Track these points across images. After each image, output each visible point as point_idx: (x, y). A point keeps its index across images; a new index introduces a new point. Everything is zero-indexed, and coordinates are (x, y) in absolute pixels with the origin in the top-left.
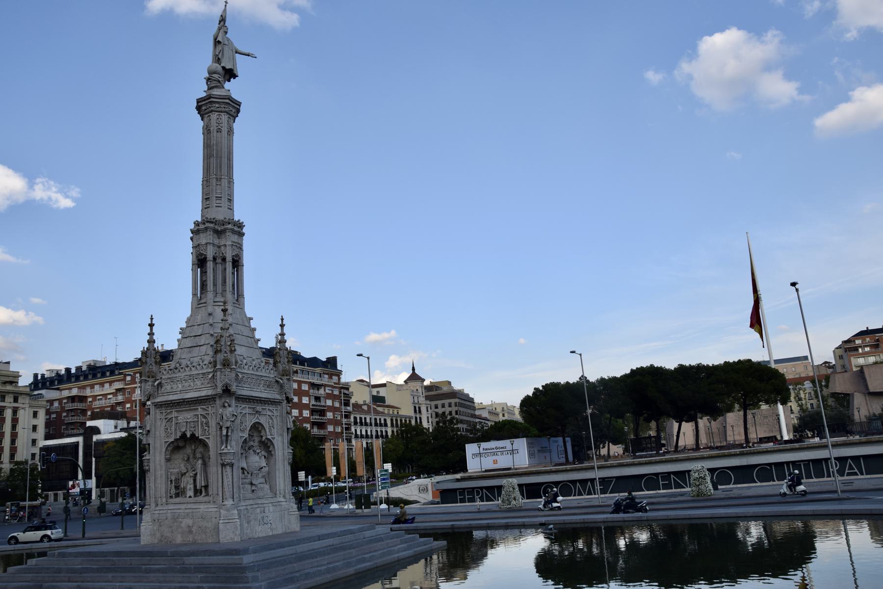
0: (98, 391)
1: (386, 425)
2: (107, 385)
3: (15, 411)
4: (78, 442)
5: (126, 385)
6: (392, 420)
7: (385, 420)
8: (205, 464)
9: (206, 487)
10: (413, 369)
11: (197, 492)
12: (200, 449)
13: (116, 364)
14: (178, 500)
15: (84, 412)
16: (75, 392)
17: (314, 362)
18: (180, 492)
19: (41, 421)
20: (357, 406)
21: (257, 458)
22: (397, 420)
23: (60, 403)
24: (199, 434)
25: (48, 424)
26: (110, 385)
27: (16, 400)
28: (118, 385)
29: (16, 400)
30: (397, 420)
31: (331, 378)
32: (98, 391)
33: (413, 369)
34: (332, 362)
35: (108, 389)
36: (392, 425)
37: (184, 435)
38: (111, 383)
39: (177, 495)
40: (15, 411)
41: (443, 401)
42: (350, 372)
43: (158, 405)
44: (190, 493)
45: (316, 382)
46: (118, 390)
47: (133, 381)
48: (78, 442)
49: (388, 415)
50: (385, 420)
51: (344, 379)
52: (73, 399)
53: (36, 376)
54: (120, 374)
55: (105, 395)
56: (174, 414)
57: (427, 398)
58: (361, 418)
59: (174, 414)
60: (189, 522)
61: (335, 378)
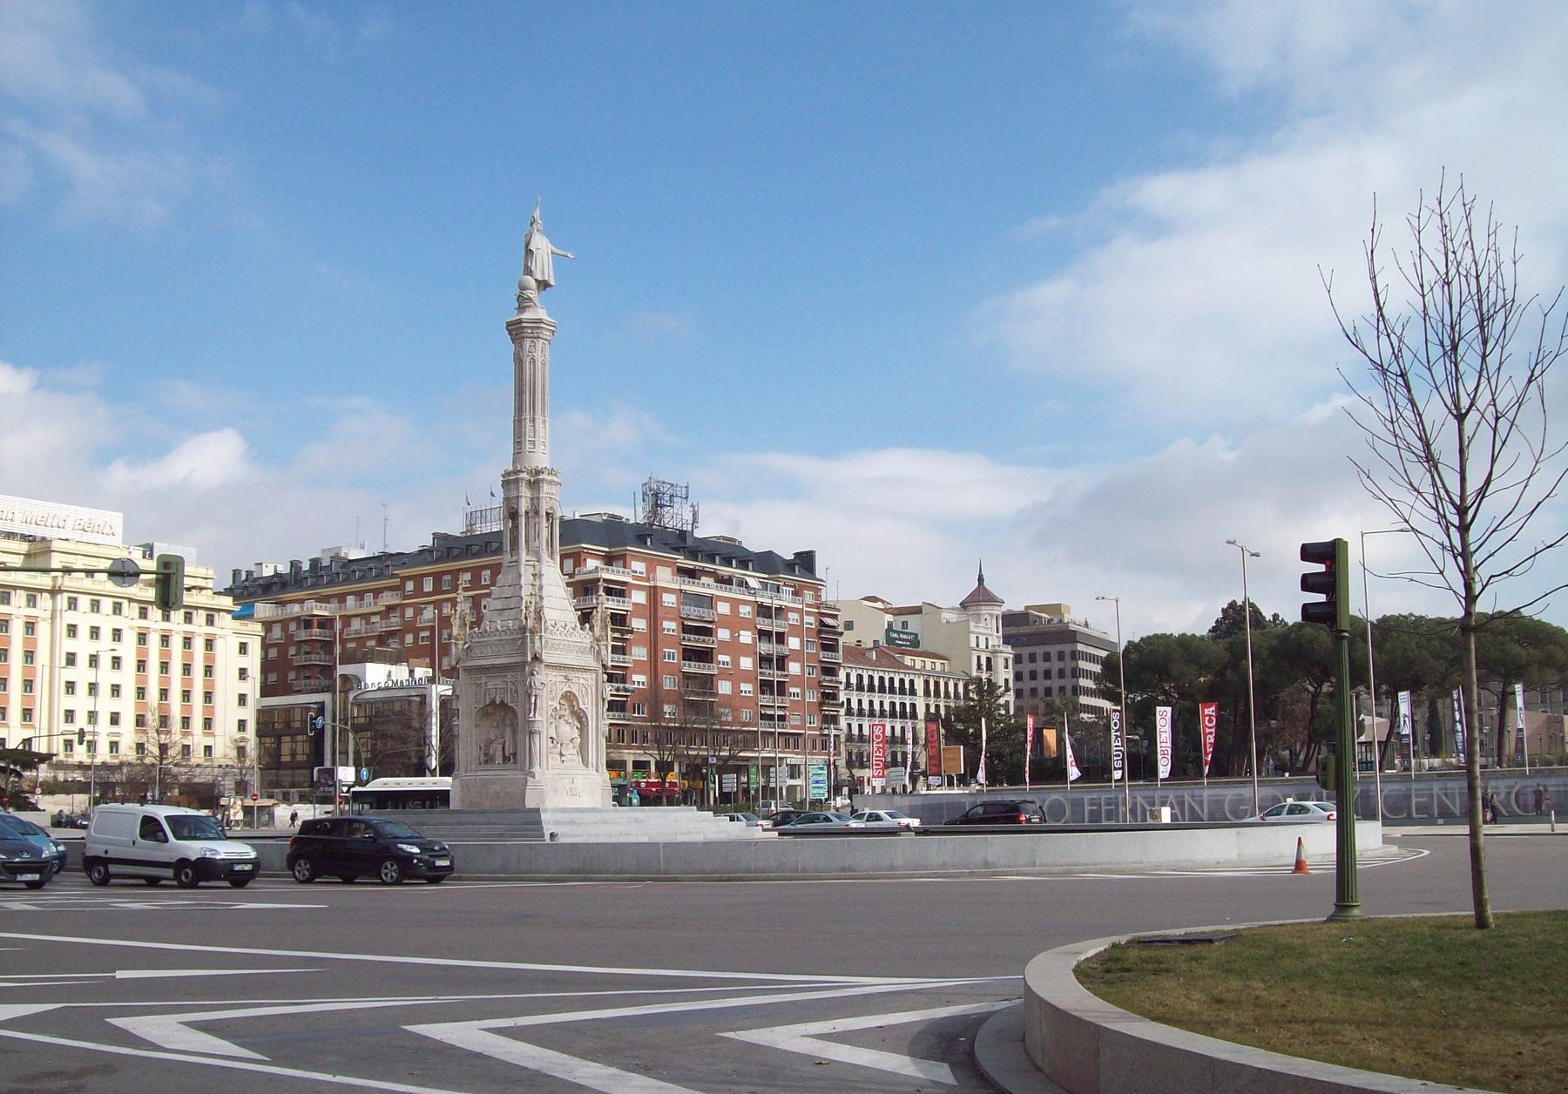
1: (913, 692)
2: (369, 597)
3: (209, 644)
4: (323, 703)
5: (406, 597)
6: (927, 683)
7: (912, 682)
8: (514, 732)
9: (515, 754)
10: (981, 579)
11: (506, 759)
12: (510, 716)
13: (386, 556)
14: (489, 766)
15: (328, 646)
17: (767, 562)
18: (489, 759)
19: (253, 661)
20: (857, 654)
21: (568, 728)
22: (937, 684)
23: (285, 628)
24: (508, 701)
25: (266, 667)
26: (375, 597)
27: (210, 621)
28: (389, 599)
29: (210, 621)
30: (937, 684)
31: (796, 593)
33: (981, 579)
34: (805, 561)
35: (369, 605)
36: (927, 693)
37: (493, 703)
38: (377, 592)
39: (486, 762)
40: (209, 644)
41: (1047, 648)
42: (840, 583)
43: (468, 670)
44: (499, 759)
45: (767, 601)
46: (390, 608)
47: (419, 591)
48: (323, 703)
49: (920, 672)
50: (912, 682)
51: (828, 595)
52: (307, 623)
53: (236, 573)
54: (394, 576)
55: (366, 617)
56: (484, 679)
57: (1007, 640)
58: (882, 679)
59: (484, 679)
60: (498, 788)
61: (808, 596)
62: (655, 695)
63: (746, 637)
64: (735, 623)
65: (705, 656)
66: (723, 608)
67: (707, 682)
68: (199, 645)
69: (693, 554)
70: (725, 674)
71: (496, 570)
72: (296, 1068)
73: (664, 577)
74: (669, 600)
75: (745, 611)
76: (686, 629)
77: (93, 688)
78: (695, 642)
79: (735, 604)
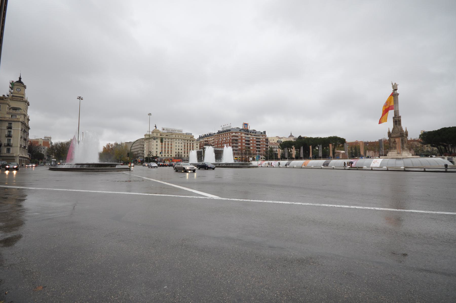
0: (210, 139)
3: (193, 144)
16: (206, 140)
19: (198, 146)
28: (212, 139)
32: (210, 139)
40: (193, 144)
42: (268, 135)
52: (205, 141)
61: (264, 137)
62: (241, 150)
63: (255, 142)
64: (253, 140)
65: (249, 144)
66: (251, 138)
67: (249, 147)
68: (192, 144)
69: (248, 132)
70: (251, 146)
71: (311, 258)
72: (174, 187)
73: (243, 135)
74: (244, 138)
75: (255, 139)
76: (246, 141)
77: (179, 146)
78: (247, 142)
79: (253, 138)
